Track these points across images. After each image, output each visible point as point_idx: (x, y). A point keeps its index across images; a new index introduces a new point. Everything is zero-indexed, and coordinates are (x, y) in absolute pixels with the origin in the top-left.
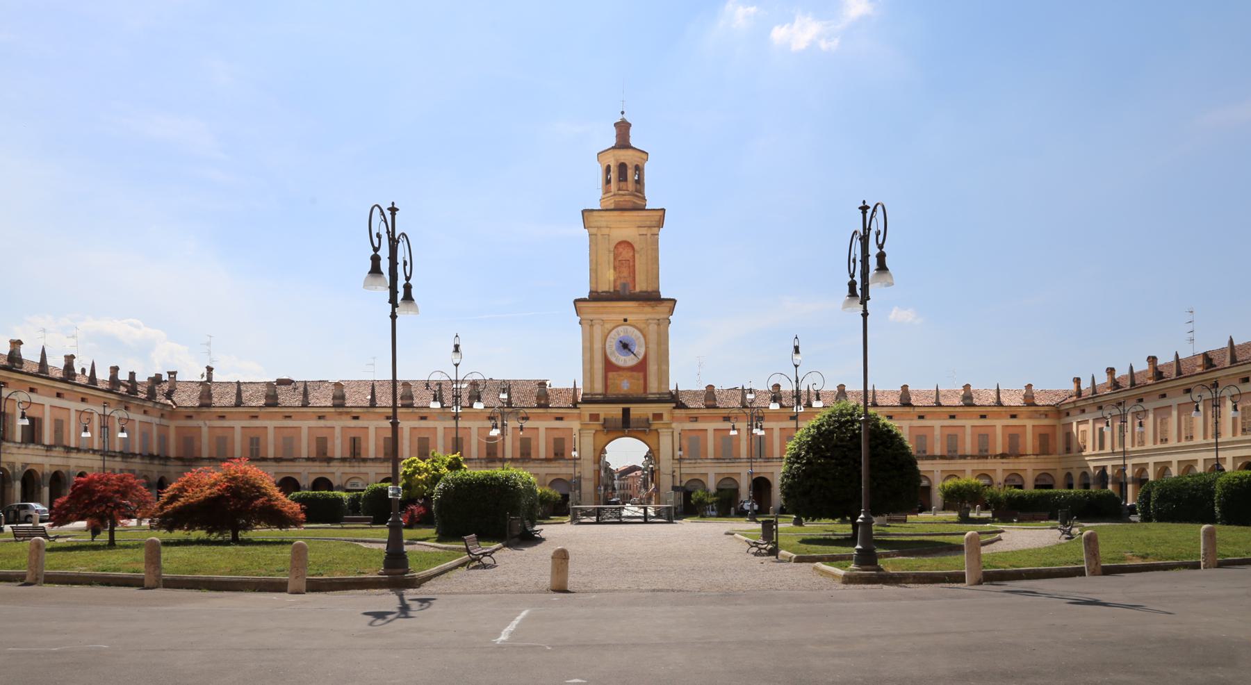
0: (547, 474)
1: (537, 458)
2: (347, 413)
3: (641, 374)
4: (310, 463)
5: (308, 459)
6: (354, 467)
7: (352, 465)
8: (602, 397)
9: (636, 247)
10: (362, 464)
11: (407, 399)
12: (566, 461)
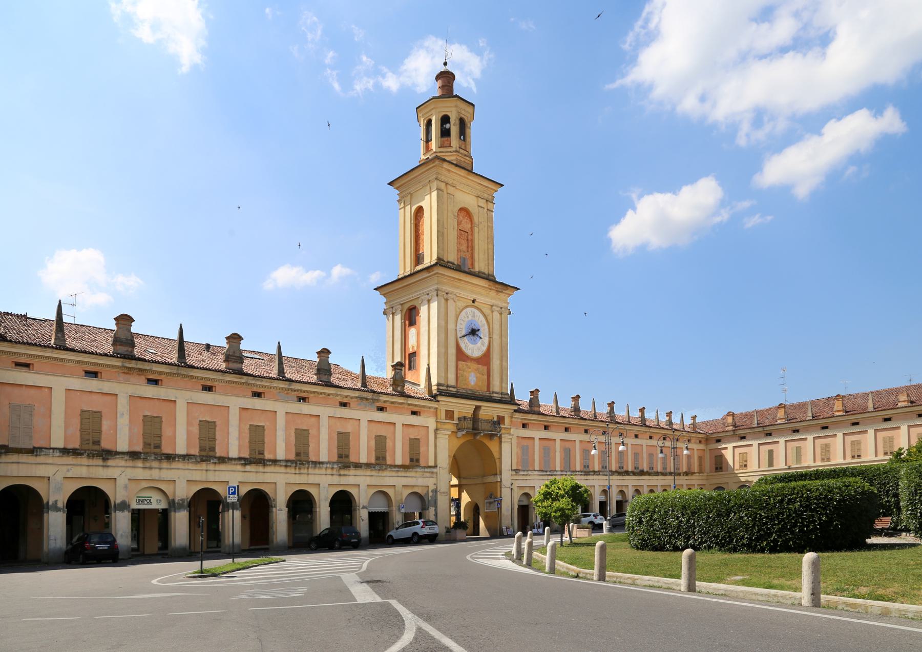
1: (427, 465)
3: (485, 368)
5: (65, 451)
6: (151, 468)
7: (148, 465)
9: (476, 219)
10: (165, 465)
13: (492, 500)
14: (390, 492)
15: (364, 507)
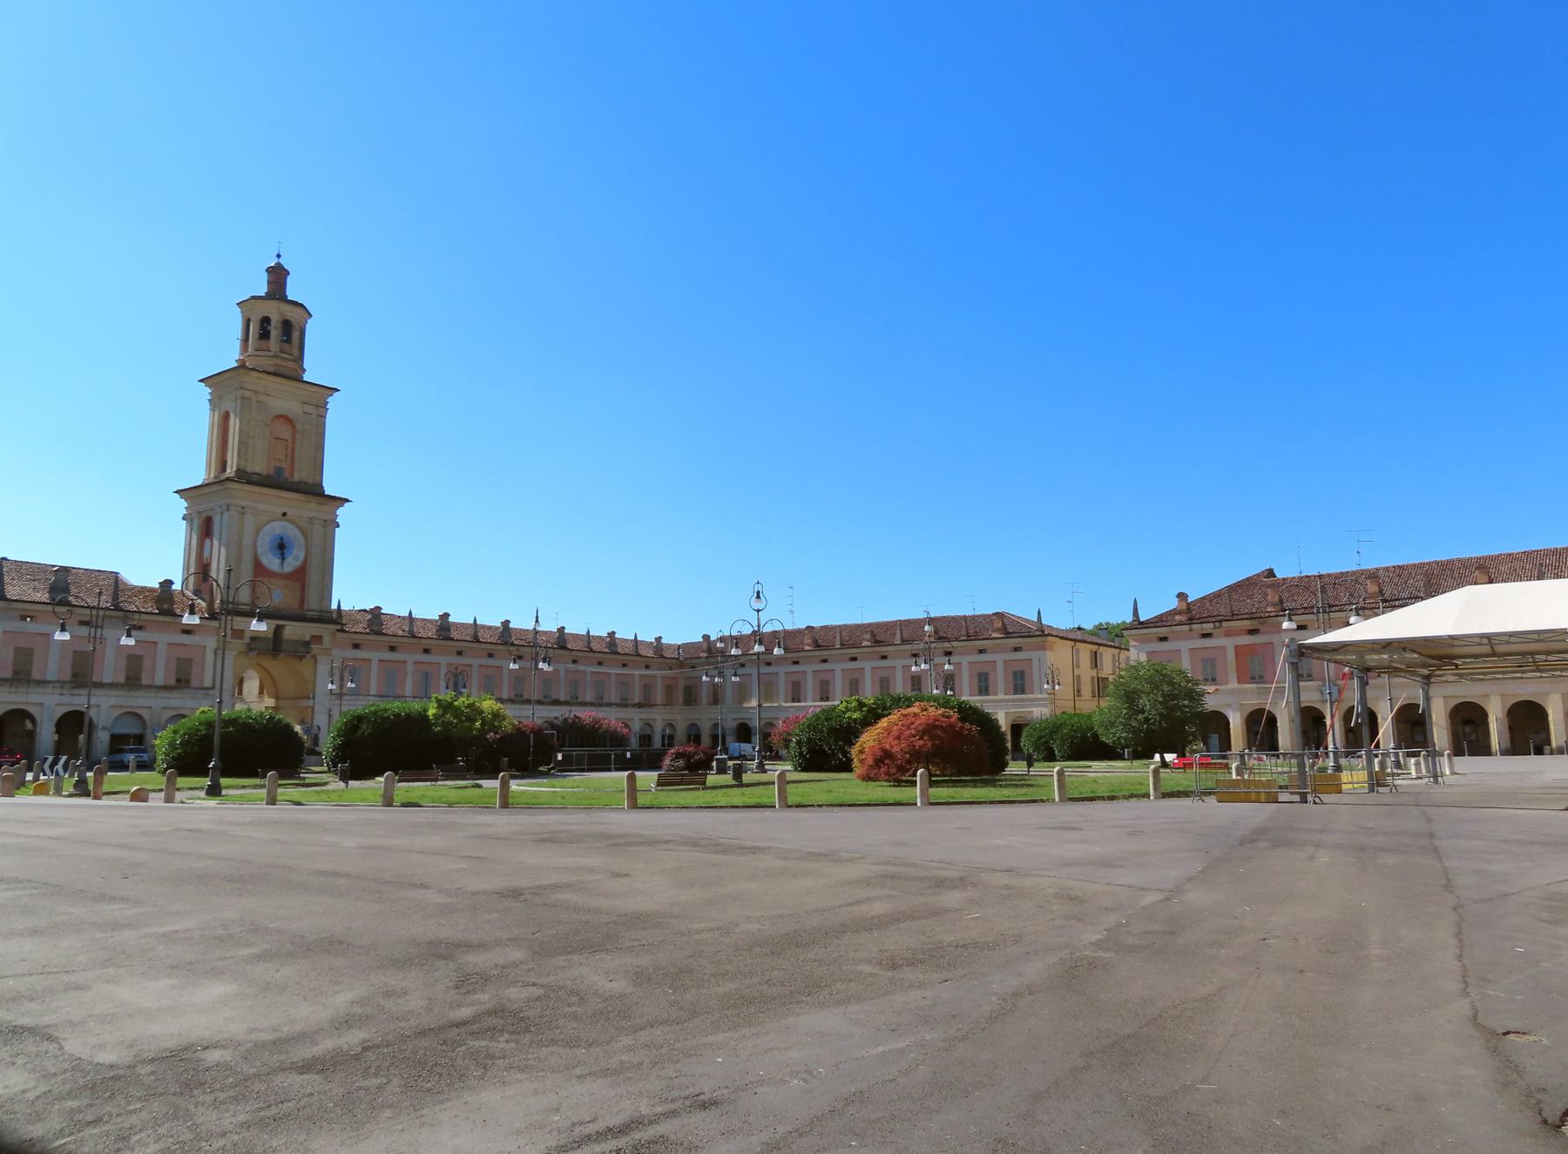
0: (164, 708)
1: (150, 683)
4: (164, 694)
8: (249, 607)
12: (194, 691)
13: (1539, 1096)
14: (143, 713)
15: (104, 728)
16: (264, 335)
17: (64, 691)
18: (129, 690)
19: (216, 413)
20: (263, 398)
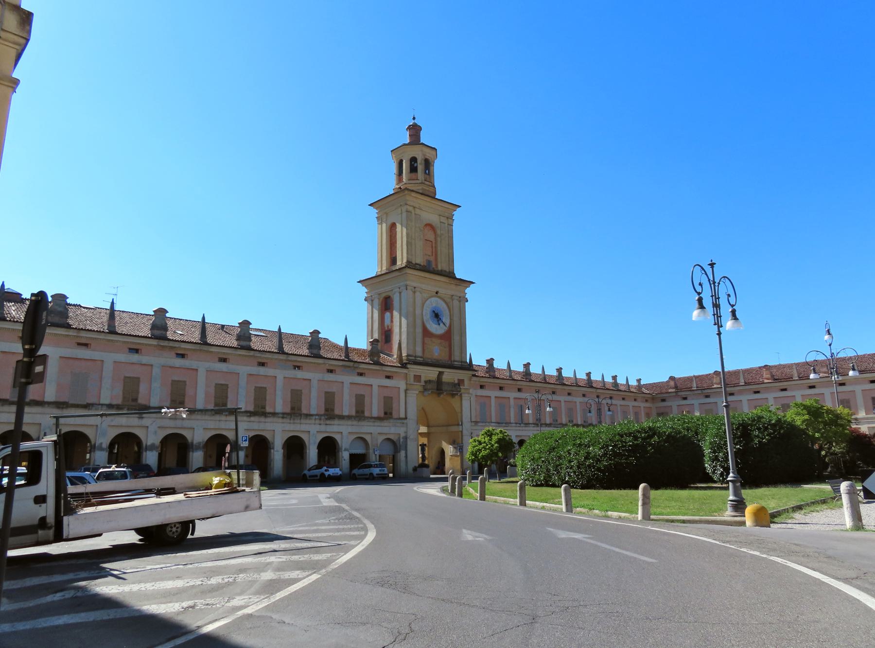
2: (172, 348)
4: (378, 423)
11: (245, 340)
12: (395, 421)
14: (368, 438)
15: (345, 450)
16: (413, 169)
17: (322, 422)
18: (359, 421)
19: (384, 225)
20: (418, 211)
